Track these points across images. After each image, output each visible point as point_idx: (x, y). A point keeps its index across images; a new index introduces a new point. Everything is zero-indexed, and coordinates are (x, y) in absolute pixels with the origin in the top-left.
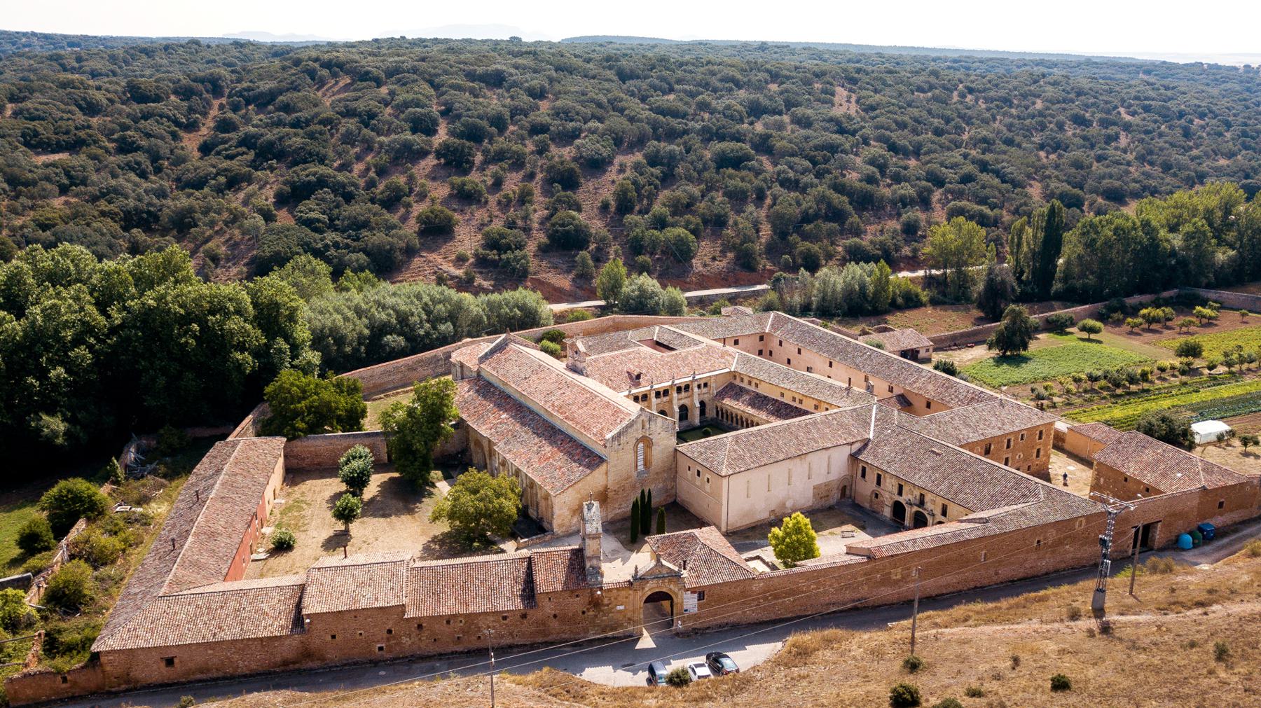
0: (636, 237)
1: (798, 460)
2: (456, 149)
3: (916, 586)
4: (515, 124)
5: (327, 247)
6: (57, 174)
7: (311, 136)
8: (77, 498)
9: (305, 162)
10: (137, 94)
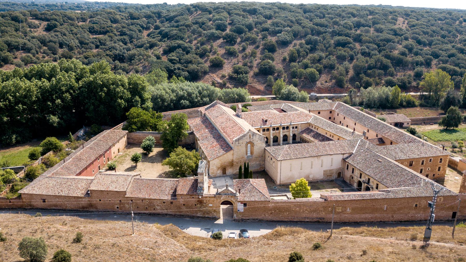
0: (293, 72)
1: (316, 158)
2: (230, 36)
3: (348, 215)
4: (256, 28)
5: (175, 69)
6: (96, 41)
7: (180, 30)
8: (51, 144)
9: (176, 39)
10: (132, 17)
